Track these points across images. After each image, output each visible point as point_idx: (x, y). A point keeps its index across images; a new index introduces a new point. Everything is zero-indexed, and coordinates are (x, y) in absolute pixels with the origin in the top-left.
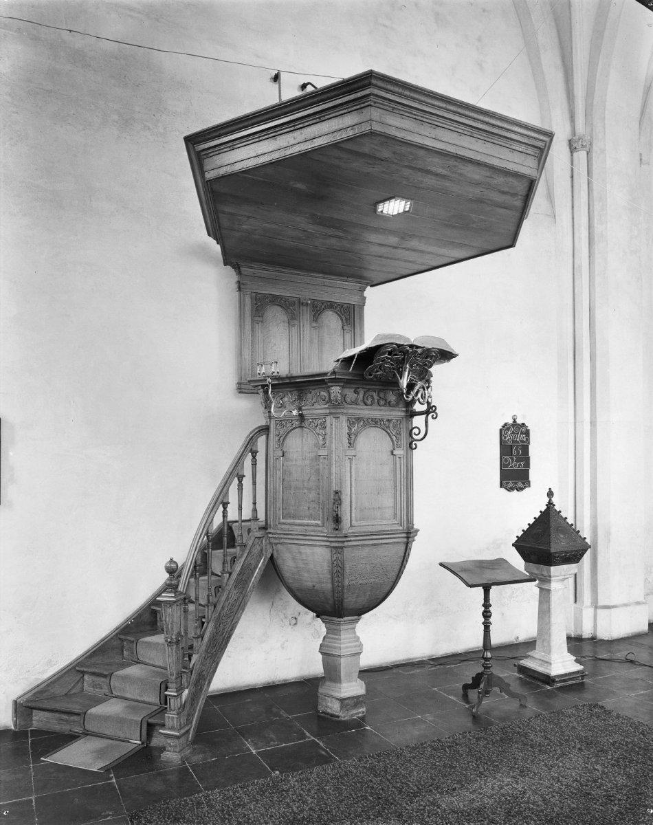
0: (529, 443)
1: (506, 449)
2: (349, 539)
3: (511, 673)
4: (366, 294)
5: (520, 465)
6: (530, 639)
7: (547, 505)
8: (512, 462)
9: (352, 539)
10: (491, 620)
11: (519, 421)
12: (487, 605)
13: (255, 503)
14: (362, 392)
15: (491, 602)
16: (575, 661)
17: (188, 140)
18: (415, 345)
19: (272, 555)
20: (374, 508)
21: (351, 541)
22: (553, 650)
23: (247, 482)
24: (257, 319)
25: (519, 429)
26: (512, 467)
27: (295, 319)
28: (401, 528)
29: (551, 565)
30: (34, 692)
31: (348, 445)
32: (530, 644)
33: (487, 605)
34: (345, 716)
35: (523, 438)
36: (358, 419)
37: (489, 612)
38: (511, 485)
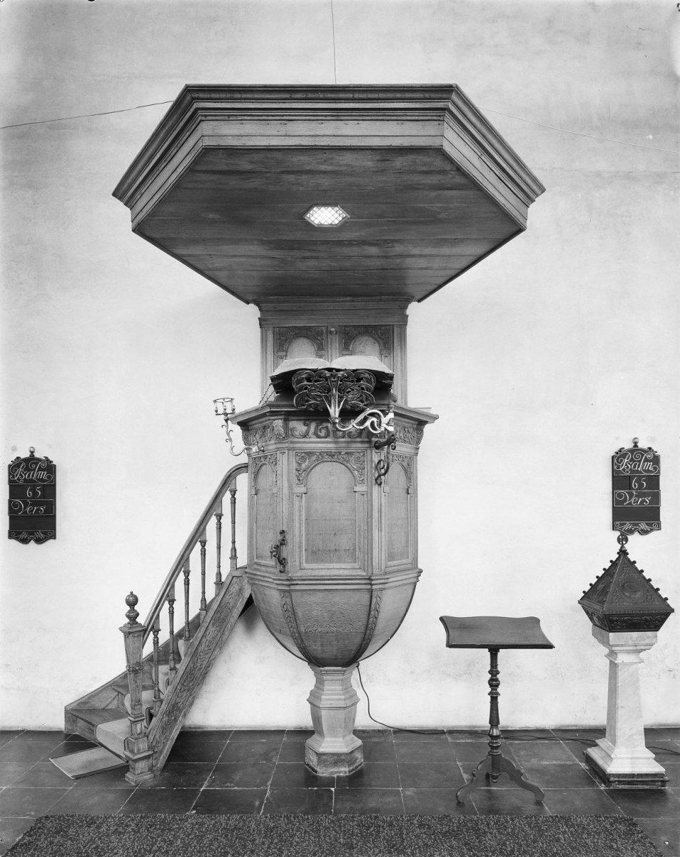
0: (659, 472)
1: (620, 481)
2: (295, 582)
3: (578, 762)
4: (408, 312)
5: (38, 510)
6: (659, 725)
7: (618, 553)
8: (630, 498)
9: (299, 582)
10: (499, 690)
11: (643, 445)
12: (494, 671)
13: (234, 542)
14: (313, 426)
15: (499, 668)
16: (655, 759)
17: (114, 194)
18: (334, 369)
19: (251, 595)
20: (329, 550)
21: (297, 584)
22: (619, 741)
23: (226, 520)
24: (280, 354)
25: (643, 455)
26: (630, 504)
27: (323, 349)
28: (364, 574)
29: (611, 631)
30: (78, 702)
31: (297, 482)
32: (600, 732)
33: (494, 671)
34: (323, 772)
35: (650, 466)
36: (310, 454)
37: (497, 680)
38: (24, 535)
